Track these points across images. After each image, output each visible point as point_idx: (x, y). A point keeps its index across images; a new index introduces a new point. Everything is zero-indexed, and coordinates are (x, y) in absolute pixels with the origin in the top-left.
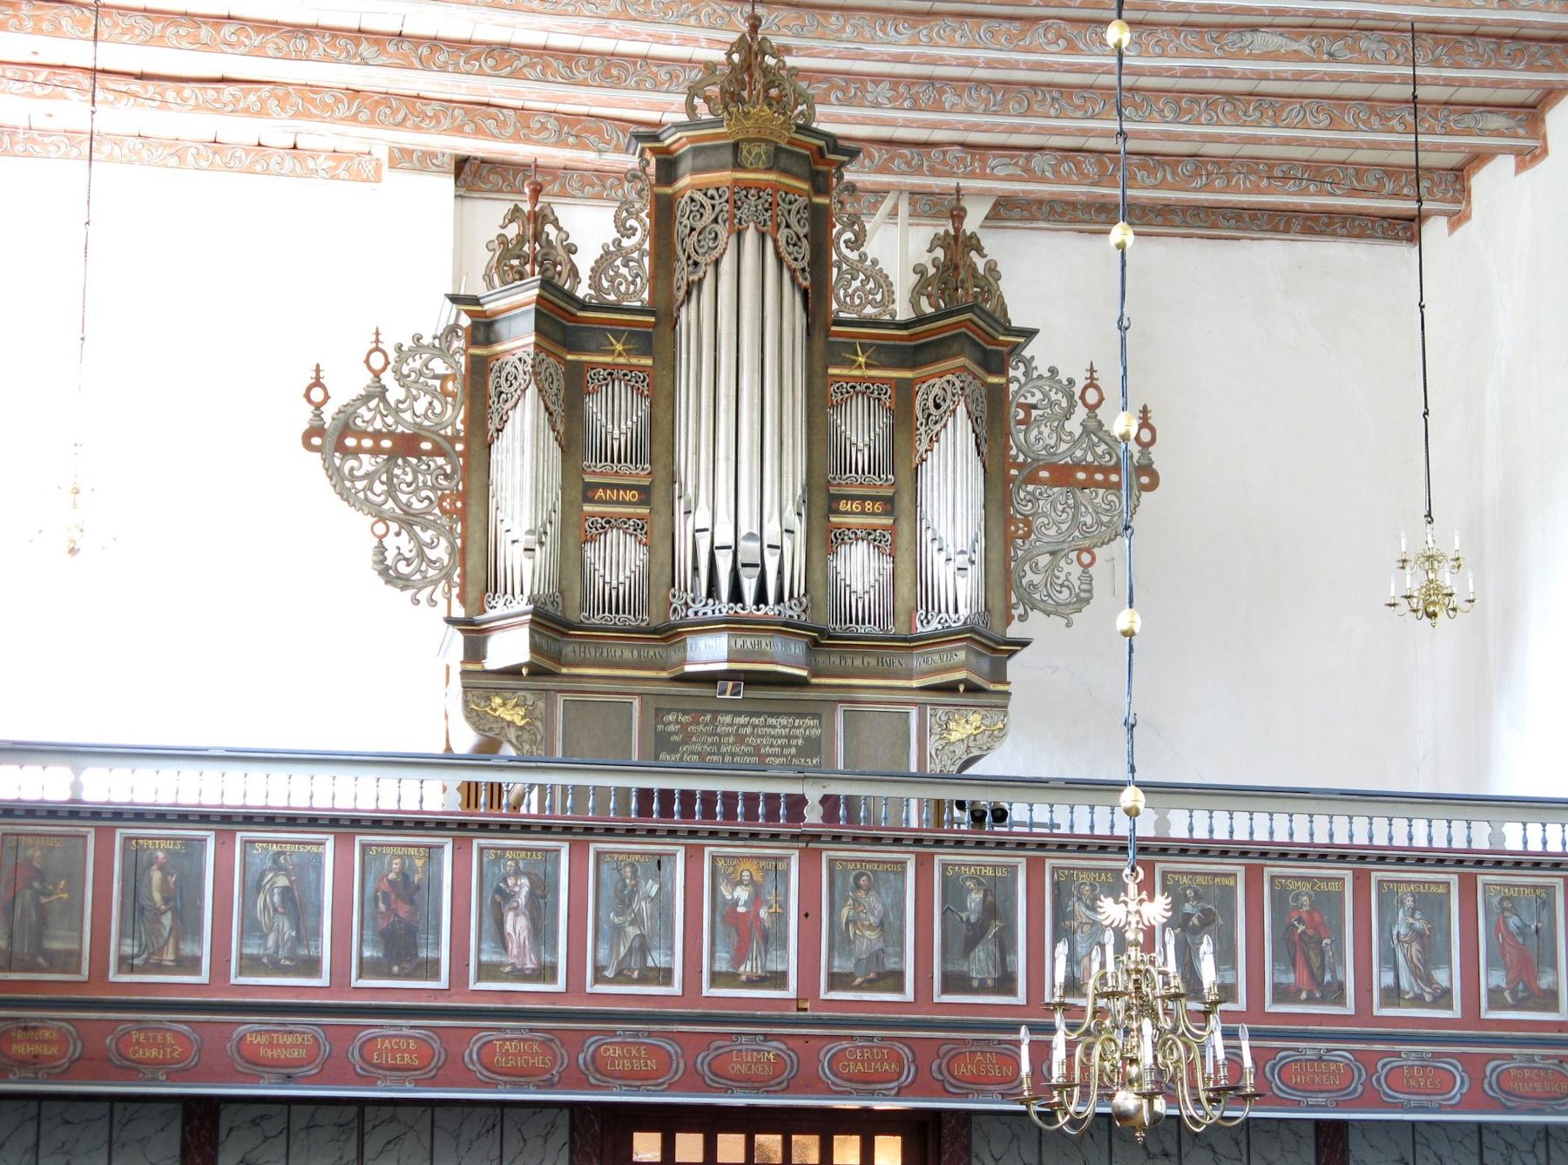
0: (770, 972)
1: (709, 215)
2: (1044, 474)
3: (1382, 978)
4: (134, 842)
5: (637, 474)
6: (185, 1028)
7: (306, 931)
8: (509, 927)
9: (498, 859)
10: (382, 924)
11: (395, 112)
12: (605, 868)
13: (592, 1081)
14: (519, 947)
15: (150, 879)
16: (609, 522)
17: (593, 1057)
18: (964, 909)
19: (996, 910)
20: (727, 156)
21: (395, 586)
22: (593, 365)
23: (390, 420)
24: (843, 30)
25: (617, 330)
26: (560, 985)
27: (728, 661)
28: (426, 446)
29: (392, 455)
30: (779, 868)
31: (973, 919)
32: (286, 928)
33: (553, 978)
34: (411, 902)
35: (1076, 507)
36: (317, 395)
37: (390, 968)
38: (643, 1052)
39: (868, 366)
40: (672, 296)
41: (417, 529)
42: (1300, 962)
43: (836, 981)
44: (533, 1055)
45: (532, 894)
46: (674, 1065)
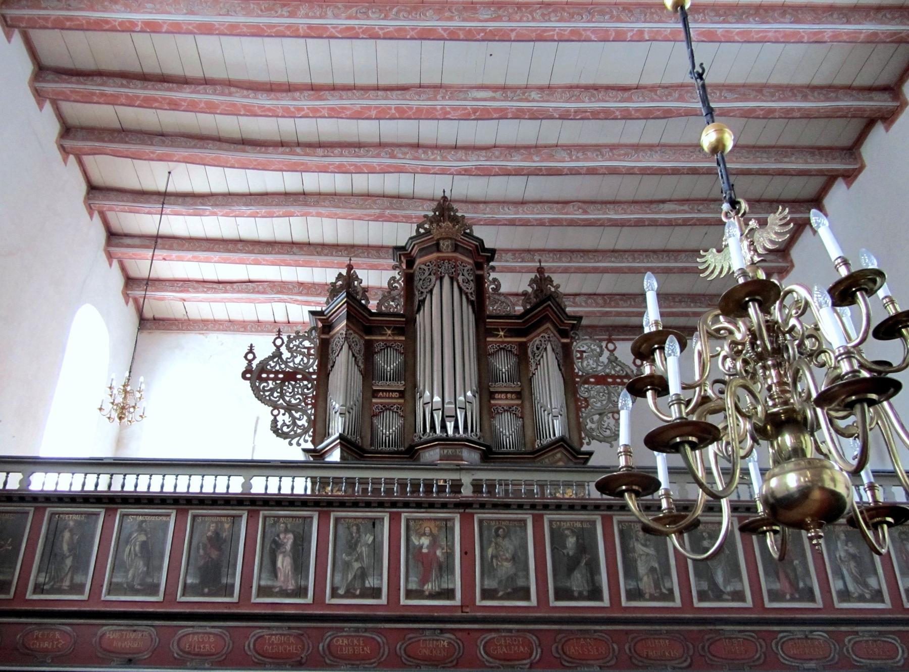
0: (444, 589)
1: (427, 273)
2: (592, 380)
3: (836, 585)
4: (57, 516)
5: (400, 386)
6: (68, 628)
7: (152, 566)
8: (279, 564)
9: (275, 523)
10: (201, 563)
11: (317, 290)
12: (340, 527)
13: (328, 661)
14: (285, 576)
15: (63, 537)
16: (386, 408)
17: (329, 645)
18: (565, 547)
19: (586, 547)
20: (435, 248)
21: (281, 437)
22: (378, 341)
23: (283, 366)
24: (486, 209)
25: (388, 324)
26: (309, 599)
27: (440, 460)
28: (299, 376)
29: (283, 381)
30: (448, 525)
31: (571, 553)
32: (141, 565)
33: (305, 595)
34: (220, 549)
35: (609, 394)
36: (250, 356)
37: (203, 590)
38: (361, 642)
39: (505, 336)
40: (413, 311)
41: (293, 412)
42: (782, 575)
43: (487, 594)
44: (289, 645)
45: (295, 544)
46: (382, 651)
